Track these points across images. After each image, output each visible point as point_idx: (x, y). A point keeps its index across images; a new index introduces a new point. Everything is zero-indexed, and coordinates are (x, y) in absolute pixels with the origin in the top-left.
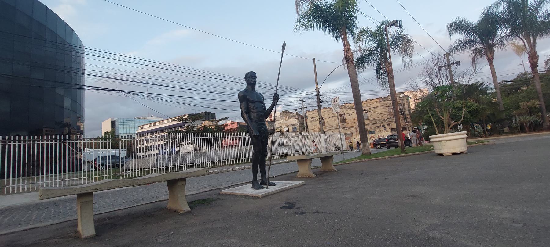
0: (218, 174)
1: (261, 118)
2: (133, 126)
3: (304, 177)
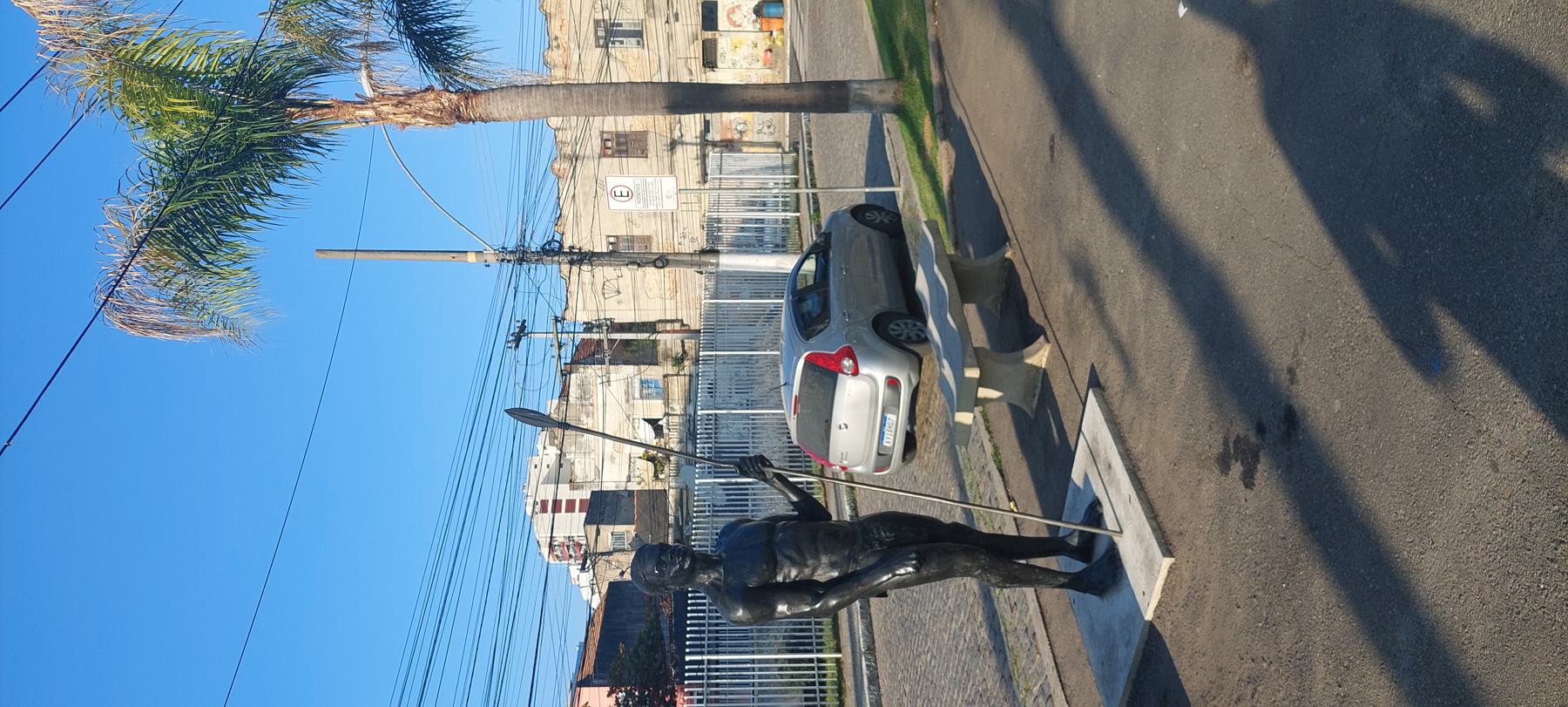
3: (1039, 385)
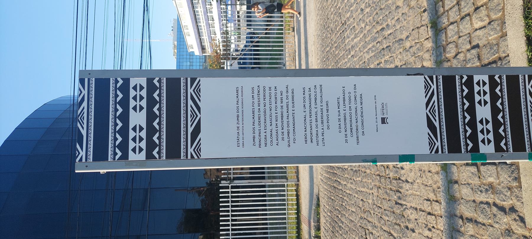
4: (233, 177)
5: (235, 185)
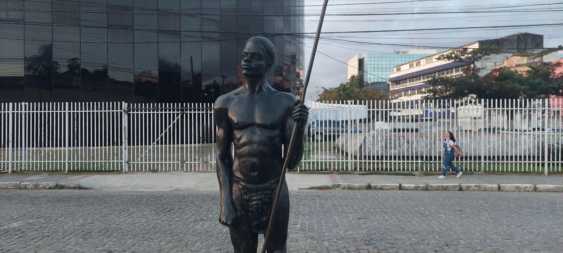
0: (460, 192)
1: (252, 174)
2: (388, 66)
4: (130, 114)
5: (123, 115)
